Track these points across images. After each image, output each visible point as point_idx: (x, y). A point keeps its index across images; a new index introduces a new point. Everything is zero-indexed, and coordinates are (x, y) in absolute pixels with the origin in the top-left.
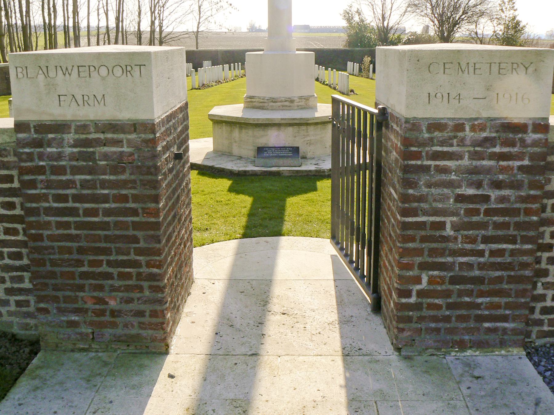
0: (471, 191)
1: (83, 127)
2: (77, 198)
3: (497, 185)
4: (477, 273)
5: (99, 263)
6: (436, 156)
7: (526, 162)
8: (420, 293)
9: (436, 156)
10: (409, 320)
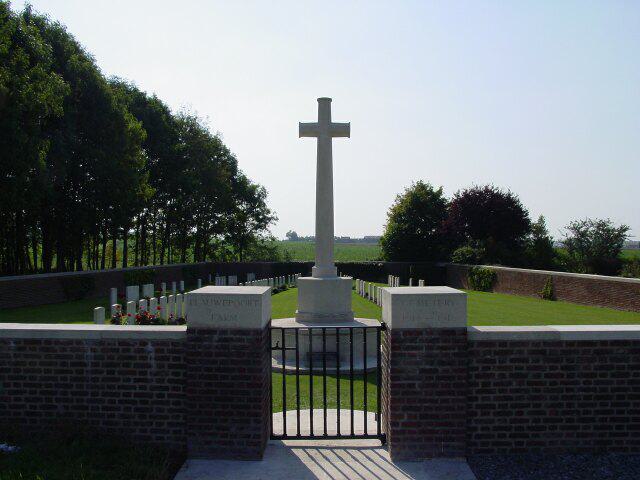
0: (428, 367)
1: (224, 332)
2: (218, 370)
3: (442, 363)
4: (434, 412)
5: (129, 380)
6: (407, 348)
7: (456, 351)
8: (404, 424)
9: (407, 348)
10: (399, 440)
